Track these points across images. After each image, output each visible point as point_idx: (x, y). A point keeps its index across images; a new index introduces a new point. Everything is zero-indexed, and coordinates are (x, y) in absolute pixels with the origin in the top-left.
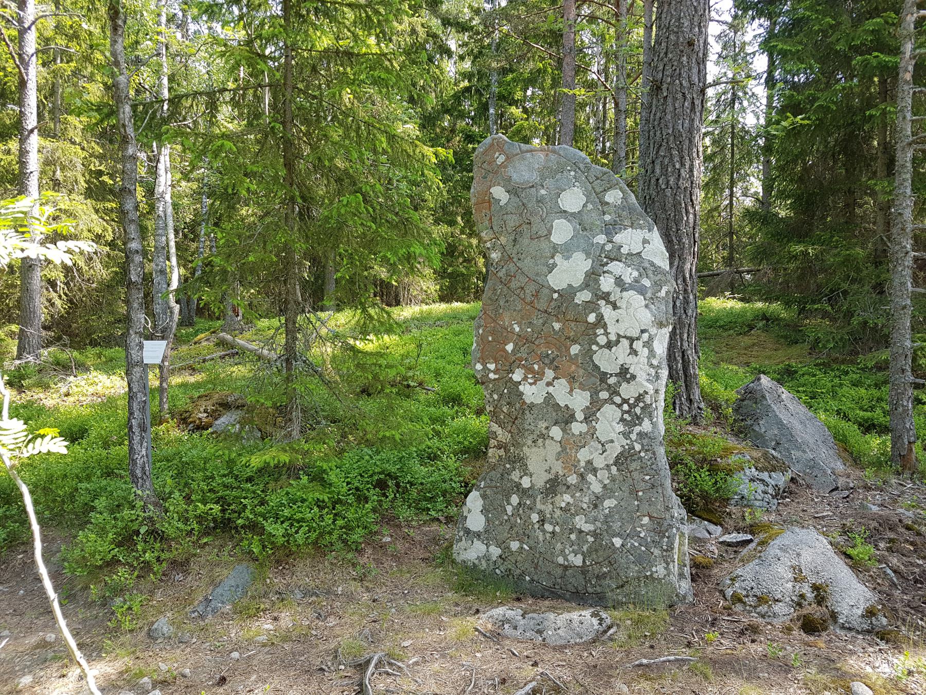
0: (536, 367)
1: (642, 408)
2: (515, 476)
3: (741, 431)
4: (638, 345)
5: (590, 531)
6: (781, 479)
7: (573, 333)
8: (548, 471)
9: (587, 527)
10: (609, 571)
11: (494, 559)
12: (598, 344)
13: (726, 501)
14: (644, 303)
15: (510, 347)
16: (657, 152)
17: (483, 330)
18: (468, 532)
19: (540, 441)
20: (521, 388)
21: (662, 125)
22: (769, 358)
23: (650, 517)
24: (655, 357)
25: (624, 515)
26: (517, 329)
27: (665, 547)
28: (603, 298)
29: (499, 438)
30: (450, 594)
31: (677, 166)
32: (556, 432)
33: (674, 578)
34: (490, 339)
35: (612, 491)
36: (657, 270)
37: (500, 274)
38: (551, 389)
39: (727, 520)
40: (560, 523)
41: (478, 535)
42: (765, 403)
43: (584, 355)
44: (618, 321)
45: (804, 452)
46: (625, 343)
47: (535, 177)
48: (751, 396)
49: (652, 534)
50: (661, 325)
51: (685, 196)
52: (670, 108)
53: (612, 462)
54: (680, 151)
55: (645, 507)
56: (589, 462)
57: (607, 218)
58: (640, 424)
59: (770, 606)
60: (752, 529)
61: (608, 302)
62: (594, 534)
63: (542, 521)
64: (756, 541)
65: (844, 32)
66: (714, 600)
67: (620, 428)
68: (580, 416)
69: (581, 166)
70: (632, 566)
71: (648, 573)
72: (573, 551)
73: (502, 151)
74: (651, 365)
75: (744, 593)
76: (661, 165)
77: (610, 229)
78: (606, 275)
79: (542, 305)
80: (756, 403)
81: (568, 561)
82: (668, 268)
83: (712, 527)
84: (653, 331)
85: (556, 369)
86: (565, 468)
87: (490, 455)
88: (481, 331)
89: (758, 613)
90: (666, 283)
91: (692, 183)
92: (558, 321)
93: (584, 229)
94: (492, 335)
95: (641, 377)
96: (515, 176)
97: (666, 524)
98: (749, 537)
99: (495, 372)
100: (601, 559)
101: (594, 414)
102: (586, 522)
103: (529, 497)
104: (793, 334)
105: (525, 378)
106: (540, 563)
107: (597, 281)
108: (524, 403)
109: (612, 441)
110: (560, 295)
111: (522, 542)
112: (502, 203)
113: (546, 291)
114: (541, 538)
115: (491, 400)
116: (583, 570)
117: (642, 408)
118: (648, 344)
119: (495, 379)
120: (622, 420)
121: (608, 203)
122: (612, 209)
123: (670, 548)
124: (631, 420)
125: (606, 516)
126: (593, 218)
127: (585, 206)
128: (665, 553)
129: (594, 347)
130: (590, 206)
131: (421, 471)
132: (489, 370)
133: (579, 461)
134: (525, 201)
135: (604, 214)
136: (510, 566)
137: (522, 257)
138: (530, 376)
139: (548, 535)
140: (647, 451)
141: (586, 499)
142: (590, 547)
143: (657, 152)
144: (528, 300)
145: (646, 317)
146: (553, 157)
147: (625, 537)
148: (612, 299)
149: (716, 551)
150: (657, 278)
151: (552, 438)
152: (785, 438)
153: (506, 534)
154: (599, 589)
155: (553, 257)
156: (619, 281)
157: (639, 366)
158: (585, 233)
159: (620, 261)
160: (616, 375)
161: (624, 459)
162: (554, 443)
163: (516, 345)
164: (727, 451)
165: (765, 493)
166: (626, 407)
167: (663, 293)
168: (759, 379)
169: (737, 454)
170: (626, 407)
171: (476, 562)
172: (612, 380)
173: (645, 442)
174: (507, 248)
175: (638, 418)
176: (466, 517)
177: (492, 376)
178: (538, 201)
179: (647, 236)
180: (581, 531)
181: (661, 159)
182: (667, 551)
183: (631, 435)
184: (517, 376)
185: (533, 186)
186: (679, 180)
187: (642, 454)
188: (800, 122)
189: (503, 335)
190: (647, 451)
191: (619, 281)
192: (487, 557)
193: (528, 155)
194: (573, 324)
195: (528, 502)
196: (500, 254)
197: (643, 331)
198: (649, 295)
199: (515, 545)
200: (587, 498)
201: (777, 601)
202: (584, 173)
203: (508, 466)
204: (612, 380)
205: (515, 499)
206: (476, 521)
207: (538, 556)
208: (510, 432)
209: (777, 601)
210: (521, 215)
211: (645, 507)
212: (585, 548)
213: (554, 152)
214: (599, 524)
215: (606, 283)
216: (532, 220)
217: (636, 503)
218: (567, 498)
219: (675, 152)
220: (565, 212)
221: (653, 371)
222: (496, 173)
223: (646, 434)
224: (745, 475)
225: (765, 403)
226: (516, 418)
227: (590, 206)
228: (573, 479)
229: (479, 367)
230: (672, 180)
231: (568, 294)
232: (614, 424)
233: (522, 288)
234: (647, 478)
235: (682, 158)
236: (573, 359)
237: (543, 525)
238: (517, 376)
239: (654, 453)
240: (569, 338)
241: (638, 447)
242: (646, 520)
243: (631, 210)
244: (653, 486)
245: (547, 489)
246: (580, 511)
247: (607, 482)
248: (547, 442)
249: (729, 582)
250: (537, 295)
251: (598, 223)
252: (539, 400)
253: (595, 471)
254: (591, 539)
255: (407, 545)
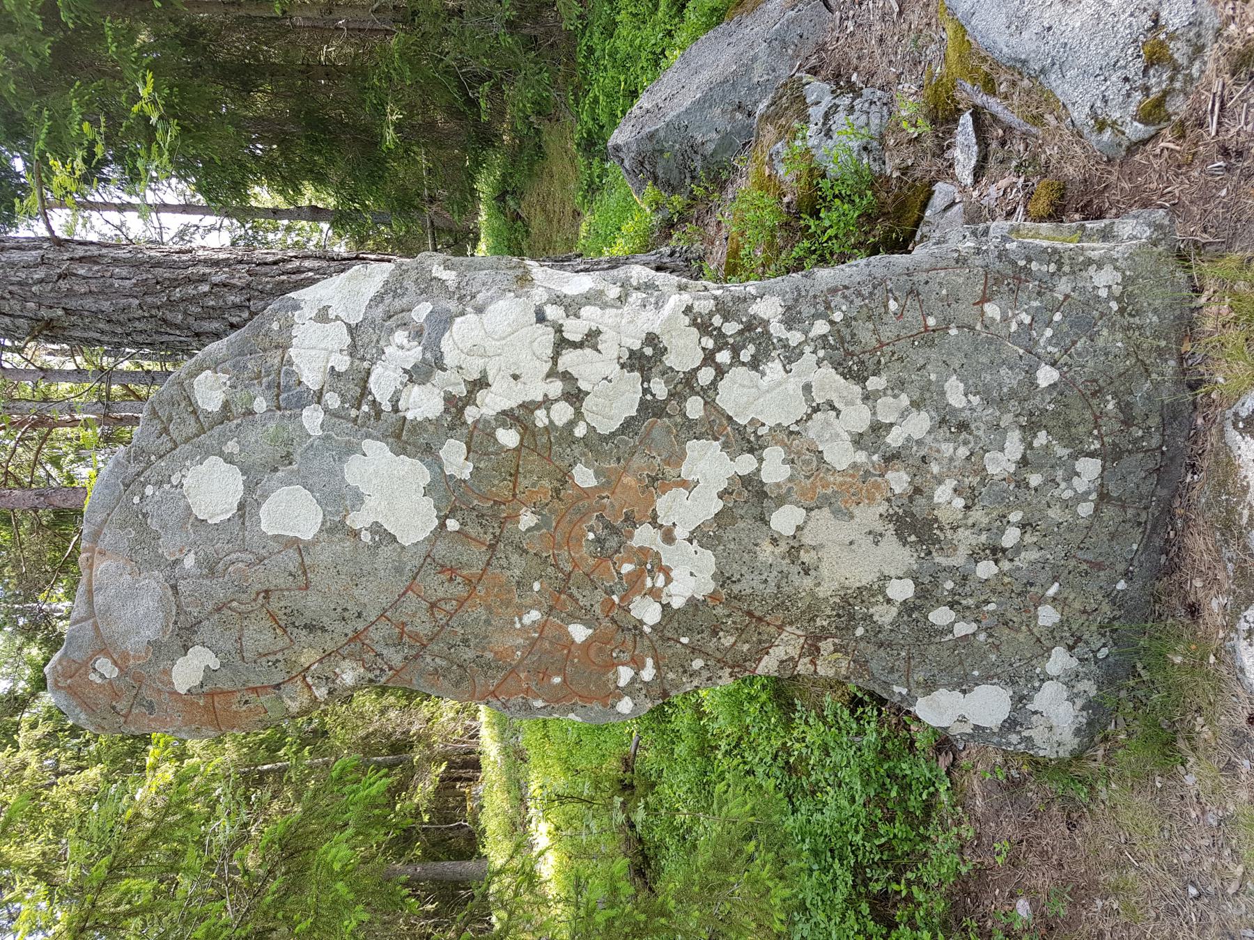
0: (627, 568)
1: (726, 319)
2: (885, 615)
3: (720, 176)
4: (574, 329)
5: (1023, 440)
6: (818, 91)
7: (545, 483)
8: (877, 537)
9: (1014, 446)
10: (1115, 395)
11: (1074, 662)
12: (571, 424)
13: (878, 182)
14: (471, 317)
15: (579, 633)
16: (177, 327)
17: (536, 697)
18: (1011, 724)
19: (804, 556)
20: (677, 603)
21: (123, 317)
22: (564, 184)
23: (985, 299)
24: (602, 292)
25: (984, 359)
26: (534, 615)
27: (1053, 267)
28: (461, 411)
29: (795, 653)
30: (1190, 780)
31: (205, 288)
32: (784, 520)
33: (1120, 250)
34: (557, 680)
35: (926, 387)
36: (392, 289)
37: (396, 659)
38: (681, 533)
39: (918, 174)
40: (1001, 510)
41: (1020, 700)
42: (662, 134)
43: (599, 456)
44: (516, 377)
45: (754, 59)
46: (569, 360)
47: (153, 582)
48: (647, 164)
49: (1023, 296)
50: (524, 279)
51: (266, 275)
52: (89, 303)
53: (857, 389)
54: (175, 283)
55: (964, 310)
56: (858, 441)
57: (260, 405)
58: (765, 323)
59: (1172, 37)
60: (943, 116)
61: (470, 399)
62: (1030, 429)
63: (996, 552)
64: (981, 99)
65: (22, 43)
66: (1156, 163)
67: (774, 369)
68: (746, 464)
69: (133, 468)
70: (1100, 342)
71: (1114, 306)
72: (1068, 479)
73: (87, 665)
74: (622, 300)
75: (1138, 96)
76: (203, 319)
77: (289, 396)
78: (401, 405)
79: (475, 556)
80: (662, 152)
81: (1088, 493)
82: (391, 266)
83: (938, 201)
84: (539, 295)
85: (631, 520)
86: (871, 499)
87: (831, 673)
88: (539, 703)
89: (1192, 61)
90: (421, 269)
91: (241, 262)
92: (514, 518)
93: (288, 458)
94: (547, 675)
95: (651, 321)
96: (149, 633)
97: (998, 265)
98: (966, 119)
99: (638, 665)
100: (1088, 415)
101: (740, 430)
102: (1002, 450)
103: (935, 582)
104: (526, 152)
105: (655, 593)
106: (1090, 556)
107: (418, 427)
108: (713, 596)
109: (807, 388)
110: (452, 513)
111: (1040, 601)
112: (214, 663)
113: (441, 549)
114: (1034, 555)
115: (705, 674)
116: (1111, 455)
117: (726, 319)
118: (572, 306)
119: (657, 666)
120: (754, 364)
121: (226, 406)
122: (241, 394)
123: (1054, 256)
124: (756, 344)
125: (988, 401)
126: (259, 440)
127: (229, 459)
128: (1066, 269)
129: (580, 431)
130: (232, 447)
131: (835, 807)
132: (633, 680)
133: (854, 466)
134: (210, 607)
135: (251, 412)
136: (1094, 628)
137: (353, 609)
138: (649, 583)
139: (1029, 539)
140: (828, 307)
141: (947, 449)
142: (1060, 439)
143: (177, 327)
144: (460, 590)
145: (506, 312)
146: (107, 539)
147: (1033, 359)
148: (461, 391)
149: (1003, 183)
150: (411, 287)
151: (799, 528)
152: (729, 93)
153: (1021, 637)
154: (1154, 421)
155: (356, 534)
156: (418, 374)
157: (625, 327)
158: (297, 457)
159: (368, 373)
160: (646, 379)
161: (851, 361)
162: (811, 524)
163: (573, 618)
164: (768, 184)
165: (851, 110)
166: (723, 357)
167: (449, 276)
168: (617, 148)
169: (772, 167)
170: (723, 357)
171: (1080, 703)
172: (660, 389)
173: (807, 310)
174: (330, 646)
175: (749, 327)
176: (976, 727)
177: (648, 674)
178: (212, 571)
179: (309, 311)
180: (1024, 462)
181: (191, 320)
182: (1060, 265)
183: (793, 343)
184: (648, 613)
185: (174, 588)
186: (234, 286)
187: (837, 317)
188: (150, 88)
189: (549, 653)
190: (828, 307)
191: (418, 374)
192: (1071, 679)
193: (99, 599)
194: (523, 482)
195: (949, 585)
196: (347, 664)
197: (541, 318)
198: (453, 306)
199: (1048, 616)
200: (944, 446)
201: (1156, 21)
202: (149, 464)
203: (860, 631)
204: (660, 389)
205: (940, 616)
206: (987, 705)
207: (1072, 563)
208: (780, 628)
209: (1156, 21)
210: (244, 615)
211: (964, 310)
212: (1062, 452)
213: (96, 536)
214: (1007, 419)
215: (424, 404)
216: (258, 587)
217: (953, 332)
218: (943, 493)
219: (177, 294)
220: (241, 506)
221: (636, 297)
222: (139, 680)
223: (789, 308)
224: (818, 147)
225: (662, 134)
226: (750, 614)
227: (232, 447)
228: (899, 481)
229: (625, 706)
230: (232, 298)
231: (449, 496)
232: (764, 383)
233: (433, 605)
234: (893, 305)
235: (189, 280)
236: (609, 482)
237: (1004, 550)
238: (648, 613)
239: (834, 291)
240: (557, 491)
241: (821, 327)
242: (992, 310)
243: (243, 351)
244: (913, 292)
245: (921, 542)
246: (974, 463)
247: (904, 400)
248: (807, 539)
249: (1107, 135)
250: (449, 571)
251: (272, 426)
252: (708, 560)
253: (878, 429)
254: (1042, 438)
255: (1032, 859)
